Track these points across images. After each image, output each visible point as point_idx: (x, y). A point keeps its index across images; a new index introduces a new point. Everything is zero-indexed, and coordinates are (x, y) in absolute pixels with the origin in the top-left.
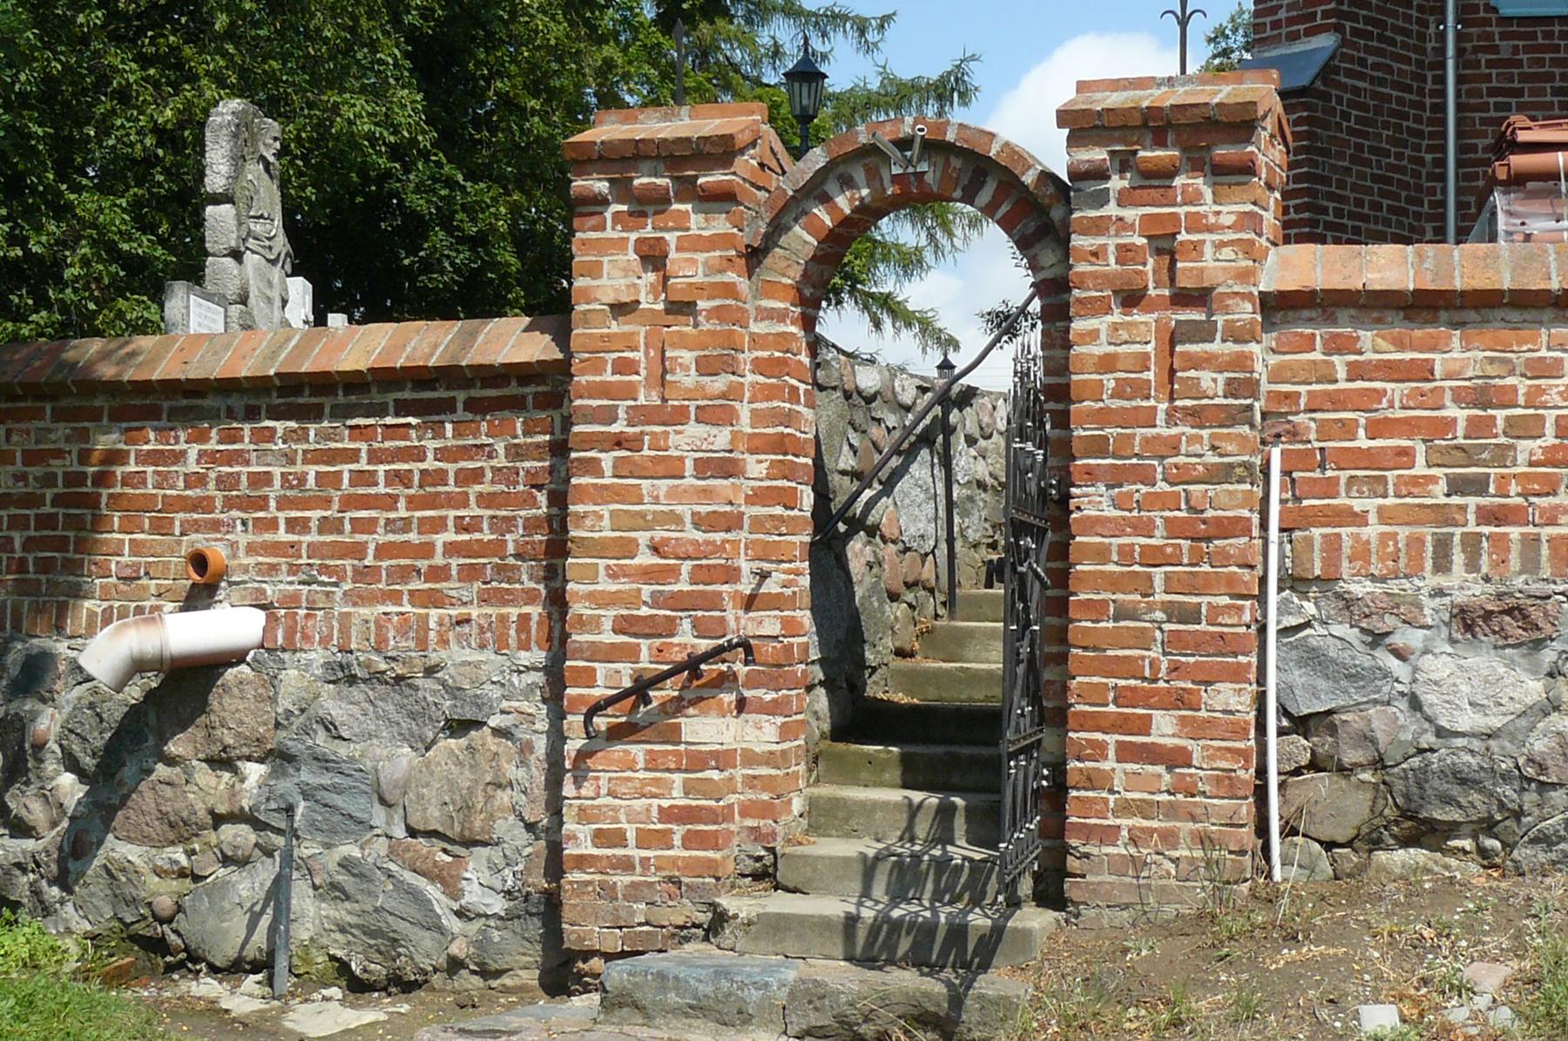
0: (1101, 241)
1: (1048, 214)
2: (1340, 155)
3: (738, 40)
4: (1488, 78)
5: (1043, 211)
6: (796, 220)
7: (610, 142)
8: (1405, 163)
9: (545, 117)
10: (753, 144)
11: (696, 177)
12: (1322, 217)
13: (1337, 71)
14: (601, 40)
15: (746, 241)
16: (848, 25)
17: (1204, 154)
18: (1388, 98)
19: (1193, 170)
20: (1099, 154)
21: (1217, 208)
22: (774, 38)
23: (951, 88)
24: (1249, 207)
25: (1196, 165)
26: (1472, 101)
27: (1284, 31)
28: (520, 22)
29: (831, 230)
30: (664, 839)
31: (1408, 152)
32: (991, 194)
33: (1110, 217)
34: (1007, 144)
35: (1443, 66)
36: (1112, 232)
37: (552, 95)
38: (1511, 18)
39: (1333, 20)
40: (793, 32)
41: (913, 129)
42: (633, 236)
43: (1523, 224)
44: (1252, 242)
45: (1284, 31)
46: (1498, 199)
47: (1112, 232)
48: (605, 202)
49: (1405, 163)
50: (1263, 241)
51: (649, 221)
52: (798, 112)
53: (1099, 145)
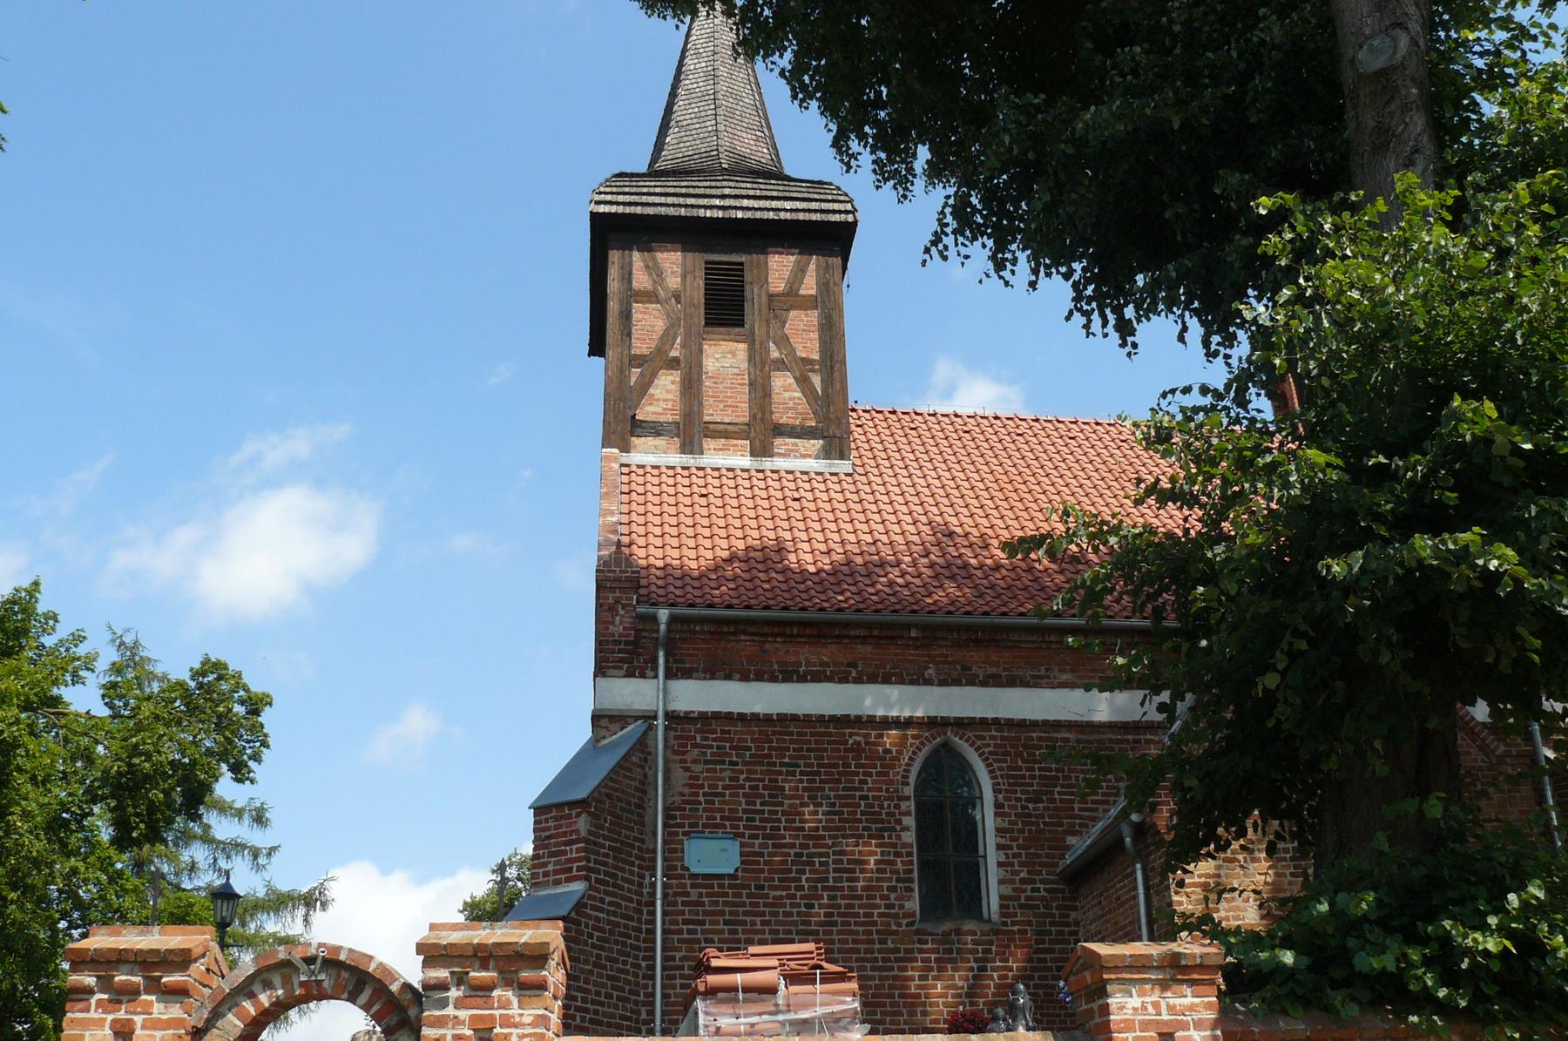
0: (442, 1031)
1: (406, 1013)
2: (586, 962)
3: (166, 857)
4: (683, 913)
5: (403, 1010)
6: (230, 1010)
7: (101, 949)
8: (628, 967)
9: (21, 908)
10: (203, 956)
11: (161, 977)
12: (573, 1003)
13: (585, 906)
14: (68, 855)
15: (193, 1023)
16: (246, 852)
17: (514, 976)
18: (617, 924)
19: (506, 986)
20: (443, 974)
21: (521, 1012)
22: (192, 857)
23: (312, 900)
24: (542, 1012)
25: (508, 983)
26: (672, 927)
27: (551, 878)
28: (11, 838)
29: (254, 1018)
31: (630, 960)
32: (368, 997)
33: (449, 1016)
34: (381, 964)
35: (653, 904)
36: (450, 1026)
37: (28, 889)
38: (699, 875)
39: (584, 873)
40: (207, 853)
41: (317, 951)
42: (110, 1017)
43: (715, 1020)
44: (543, 1035)
45: (551, 878)
46: (699, 1004)
47: (450, 1026)
48: (91, 992)
49: (628, 967)
50: (550, 1034)
51: (123, 1007)
52: (219, 920)
53: (444, 967)
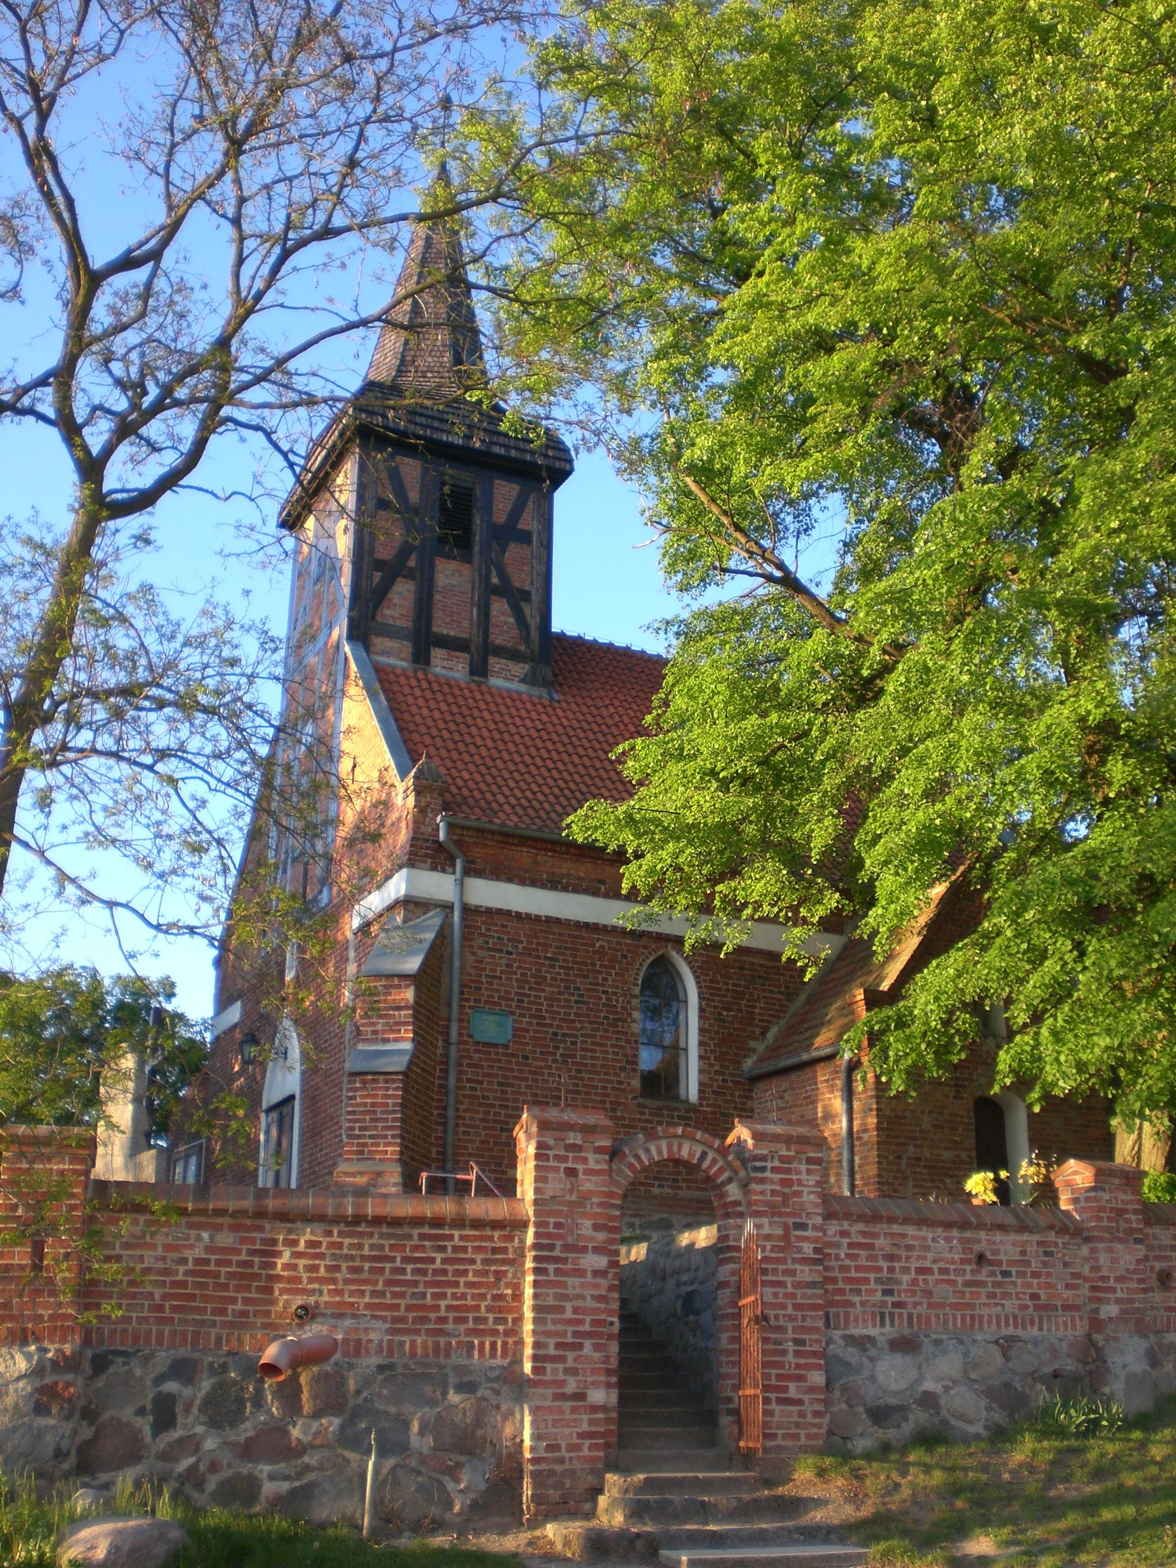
30: (577, 1447)
